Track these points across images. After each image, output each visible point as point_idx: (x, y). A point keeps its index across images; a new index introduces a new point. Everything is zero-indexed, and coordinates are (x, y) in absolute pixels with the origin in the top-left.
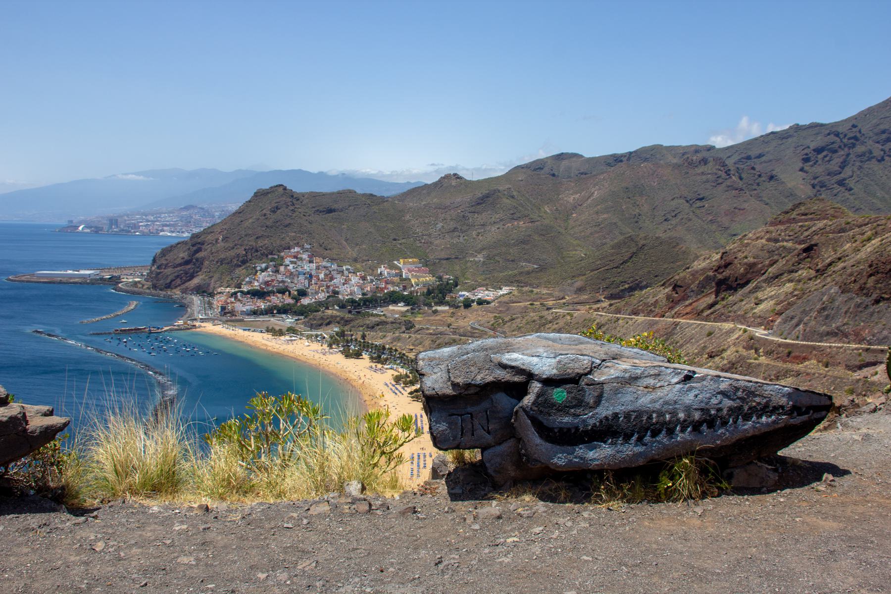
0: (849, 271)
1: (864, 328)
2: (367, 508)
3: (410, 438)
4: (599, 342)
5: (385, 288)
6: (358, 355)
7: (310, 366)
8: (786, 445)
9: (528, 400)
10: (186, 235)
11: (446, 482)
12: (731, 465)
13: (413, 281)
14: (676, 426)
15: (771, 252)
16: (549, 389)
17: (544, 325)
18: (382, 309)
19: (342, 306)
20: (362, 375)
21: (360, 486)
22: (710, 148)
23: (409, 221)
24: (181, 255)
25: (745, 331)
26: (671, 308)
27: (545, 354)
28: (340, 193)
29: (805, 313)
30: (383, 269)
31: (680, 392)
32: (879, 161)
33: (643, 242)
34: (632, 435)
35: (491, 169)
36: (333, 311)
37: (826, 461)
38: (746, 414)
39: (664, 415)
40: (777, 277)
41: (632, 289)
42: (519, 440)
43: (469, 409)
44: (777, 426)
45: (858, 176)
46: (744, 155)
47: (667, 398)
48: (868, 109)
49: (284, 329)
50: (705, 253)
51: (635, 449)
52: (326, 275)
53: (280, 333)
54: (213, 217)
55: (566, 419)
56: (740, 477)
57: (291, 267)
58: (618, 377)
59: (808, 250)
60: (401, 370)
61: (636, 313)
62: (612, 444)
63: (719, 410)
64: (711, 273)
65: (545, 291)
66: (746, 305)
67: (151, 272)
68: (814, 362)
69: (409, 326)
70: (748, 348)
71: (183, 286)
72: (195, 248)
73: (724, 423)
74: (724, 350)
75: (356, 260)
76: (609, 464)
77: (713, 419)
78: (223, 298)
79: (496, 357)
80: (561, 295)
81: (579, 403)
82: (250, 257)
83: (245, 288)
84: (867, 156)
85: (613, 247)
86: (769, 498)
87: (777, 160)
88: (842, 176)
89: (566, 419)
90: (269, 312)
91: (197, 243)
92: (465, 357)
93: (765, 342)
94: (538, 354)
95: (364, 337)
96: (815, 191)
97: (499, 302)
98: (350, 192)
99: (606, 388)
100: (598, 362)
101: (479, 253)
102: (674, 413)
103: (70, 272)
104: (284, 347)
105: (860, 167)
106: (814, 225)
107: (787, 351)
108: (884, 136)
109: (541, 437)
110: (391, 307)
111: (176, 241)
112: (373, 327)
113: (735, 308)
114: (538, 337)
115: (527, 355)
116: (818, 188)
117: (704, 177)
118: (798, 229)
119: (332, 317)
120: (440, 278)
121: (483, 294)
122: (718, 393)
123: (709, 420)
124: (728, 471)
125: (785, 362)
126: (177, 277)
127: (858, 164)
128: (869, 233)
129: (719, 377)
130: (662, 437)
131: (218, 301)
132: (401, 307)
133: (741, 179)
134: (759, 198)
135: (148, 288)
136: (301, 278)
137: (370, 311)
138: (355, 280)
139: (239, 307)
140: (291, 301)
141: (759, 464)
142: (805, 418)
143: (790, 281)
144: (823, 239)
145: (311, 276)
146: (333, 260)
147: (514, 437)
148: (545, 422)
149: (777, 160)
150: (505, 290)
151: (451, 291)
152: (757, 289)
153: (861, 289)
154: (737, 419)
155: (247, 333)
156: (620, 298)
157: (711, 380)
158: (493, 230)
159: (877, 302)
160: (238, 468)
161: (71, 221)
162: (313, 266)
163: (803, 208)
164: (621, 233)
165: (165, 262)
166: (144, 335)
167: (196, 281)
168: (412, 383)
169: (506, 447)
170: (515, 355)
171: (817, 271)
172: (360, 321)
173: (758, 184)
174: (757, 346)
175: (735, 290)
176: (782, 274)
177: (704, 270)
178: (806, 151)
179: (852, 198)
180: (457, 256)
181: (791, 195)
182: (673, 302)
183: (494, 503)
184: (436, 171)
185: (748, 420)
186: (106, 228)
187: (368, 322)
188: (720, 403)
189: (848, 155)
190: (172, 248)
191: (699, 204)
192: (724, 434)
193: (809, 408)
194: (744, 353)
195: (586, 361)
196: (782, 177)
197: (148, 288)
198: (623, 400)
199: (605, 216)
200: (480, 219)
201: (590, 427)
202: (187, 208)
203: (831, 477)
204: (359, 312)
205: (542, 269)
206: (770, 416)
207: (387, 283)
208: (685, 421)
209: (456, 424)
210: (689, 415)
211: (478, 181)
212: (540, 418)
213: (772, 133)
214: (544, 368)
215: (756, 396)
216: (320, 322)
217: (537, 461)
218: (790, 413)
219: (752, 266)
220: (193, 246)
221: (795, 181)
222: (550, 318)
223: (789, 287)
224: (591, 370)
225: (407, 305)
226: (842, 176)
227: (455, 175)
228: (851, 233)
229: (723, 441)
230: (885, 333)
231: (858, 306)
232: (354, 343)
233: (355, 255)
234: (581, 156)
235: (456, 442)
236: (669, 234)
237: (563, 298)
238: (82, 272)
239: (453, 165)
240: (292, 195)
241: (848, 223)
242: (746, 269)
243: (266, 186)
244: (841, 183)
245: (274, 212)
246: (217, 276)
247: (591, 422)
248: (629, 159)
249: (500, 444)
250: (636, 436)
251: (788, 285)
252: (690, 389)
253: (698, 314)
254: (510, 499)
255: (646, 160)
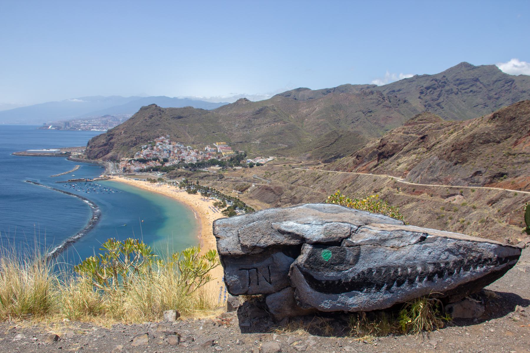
0: (442, 149)
1: (449, 177)
2: (176, 341)
3: (215, 266)
4: (354, 210)
5: (209, 157)
6: (195, 192)
7: (170, 197)
8: (488, 285)
9: (302, 259)
10: (105, 130)
11: (238, 314)
12: (451, 301)
13: (223, 154)
14: (416, 277)
15: (405, 139)
16: (318, 251)
17: (291, 176)
18: (208, 168)
19: (187, 167)
20: (197, 202)
21: (175, 314)
22: (375, 86)
23: (221, 123)
24: (102, 141)
25: (392, 179)
26: (356, 167)
27: (314, 222)
28: (185, 108)
29: (421, 169)
30: (207, 147)
31: (418, 250)
32: (456, 94)
33: (341, 134)
34: (383, 285)
35: (261, 96)
36: (182, 170)
37: (510, 292)
38: (466, 266)
39: (406, 269)
40: (408, 152)
41: (336, 158)
42: (294, 289)
43: (255, 265)
44: (486, 273)
45: (446, 101)
46: (391, 90)
47: (408, 256)
48: (451, 68)
49: (156, 179)
50: (372, 139)
51: (385, 296)
52: (178, 151)
53: (155, 181)
54: (119, 121)
55: (332, 274)
56: (458, 310)
57: (160, 147)
58: (371, 240)
59: (423, 138)
60: (217, 200)
61: (338, 170)
62: (367, 292)
63: (447, 263)
64: (375, 150)
65: (291, 159)
66: (393, 166)
67: (87, 150)
68: (426, 194)
69: (221, 177)
70: (394, 187)
71: (104, 157)
72: (109, 137)
73: (451, 274)
74: (382, 189)
75: (193, 143)
76: (364, 308)
77: (443, 271)
78: (124, 163)
79: (277, 225)
80: (300, 161)
81: (342, 261)
82: (138, 142)
83: (136, 158)
84: (450, 92)
85: (326, 136)
86: (481, 327)
87: (408, 93)
88: (439, 101)
89: (332, 274)
90: (148, 170)
91: (110, 135)
92: (251, 224)
93: (402, 184)
94: (309, 222)
95: (198, 183)
96: (426, 108)
97: (268, 165)
98: (190, 107)
99: (363, 248)
100: (356, 227)
101: (257, 139)
102: (414, 267)
103: (45, 150)
104: (157, 188)
105: (447, 97)
106: (426, 125)
107: (413, 189)
108: (458, 82)
109: (311, 287)
110: (212, 167)
111: (99, 134)
112: (202, 178)
113: (387, 167)
114: (308, 207)
115: (300, 223)
116: (427, 107)
117: (372, 101)
118: (418, 127)
119: (181, 172)
120: (237, 152)
121: (259, 160)
122: (446, 250)
123: (440, 271)
124: (449, 306)
125: (412, 194)
126: (100, 152)
127: (446, 95)
128: (452, 130)
129: (446, 238)
130: (405, 286)
131: (122, 165)
132: (217, 167)
133: (390, 102)
134: (399, 111)
135: (86, 158)
136: (165, 152)
137: (201, 169)
138: (193, 153)
139: (133, 168)
140: (160, 165)
141: (470, 299)
142: (504, 265)
143: (414, 153)
144: (430, 133)
145: (170, 151)
146: (181, 143)
147: (290, 286)
148: (315, 277)
149: (408, 93)
150: (271, 158)
151: (243, 159)
152: (398, 157)
153: (448, 157)
154: (460, 270)
155: (137, 181)
156: (330, 162)
157: (441, 240)
158: (264, 127)
159: (456, 164)
160: (92, 297)
161: (45, 124)
162: (171, 146)
163: (420, 117)
164: (330, 129)
165: (93, 145)
166: (83, 183)
167: (110, 155)
168: (223, 206)
169: (285, 293)
170: (291, 223)
171: (427, 149)
172: (196, 175)
173: (398, 105)
174: (398, 186)
175: (388, 158)
176: (410, 150)
177: (372, 148)
178: (421, 88)
179: (443, 112)
180: (246, 141)
181: (415, 110)
182: (356, 164)
183: (275, 336)
184: (234, 97)
185: (467, 271)
186: (63, 127)
187: (200, 175)
188: (447, 258)
189: (442, 91)
190: (97, 137)
191: (369, 114)
192: (451, 282)
193: (507, 258)
194: (392, 190)
195: (346, 227)
196: (410, 101)
197: (86, 158)
198: (376, 258)
199: (322, 120)
200: (258, 121)
201: (350, 280)
202: (105, 116)
203: (521, 308)
204: (195, 170)
205: (290, 147)
206: (482, 267)
207: (210, 155)
208: (422, 273)
209: (245, 276)
210: (425, 268)
211: (257, 102)
212: (311, 273)
213: (405, 79)
214: (314, 234)
215: (472, 251)
216: (175, 175)
217: (308, 305)
218: (495, 264)
219: (396, 146)
220: (109, 136)
221: (416, 103)
222: (294, 172)
223: (414, 156)
224: (351, 234)
225: (220, 166)
226: (439, 101)
227: (245, 99)
228: (443, 130)
229: (449, 287)
230: (459, 179)
231: (447, 166)
232: (193, 186)
233: (193, 140)
234: (310, 89)
235: (245, 290)
236: (355, 129)
237: (301, 162)
238: (51, 150)
239: (242, 94)
240: (160, 109)
241: (442, 125)
242: (392, 148)
243: (146, 105)
244: (438, 105)
245: (151, 118)
246: (121, 151)
247: (351, 275)
248: (334, 91)
249: (279, 291)
250: (385, 286)
251: (413, 156)
252: (425, 248)
253: (369, 171)
254: (287, 333)
255: (343, 92)
